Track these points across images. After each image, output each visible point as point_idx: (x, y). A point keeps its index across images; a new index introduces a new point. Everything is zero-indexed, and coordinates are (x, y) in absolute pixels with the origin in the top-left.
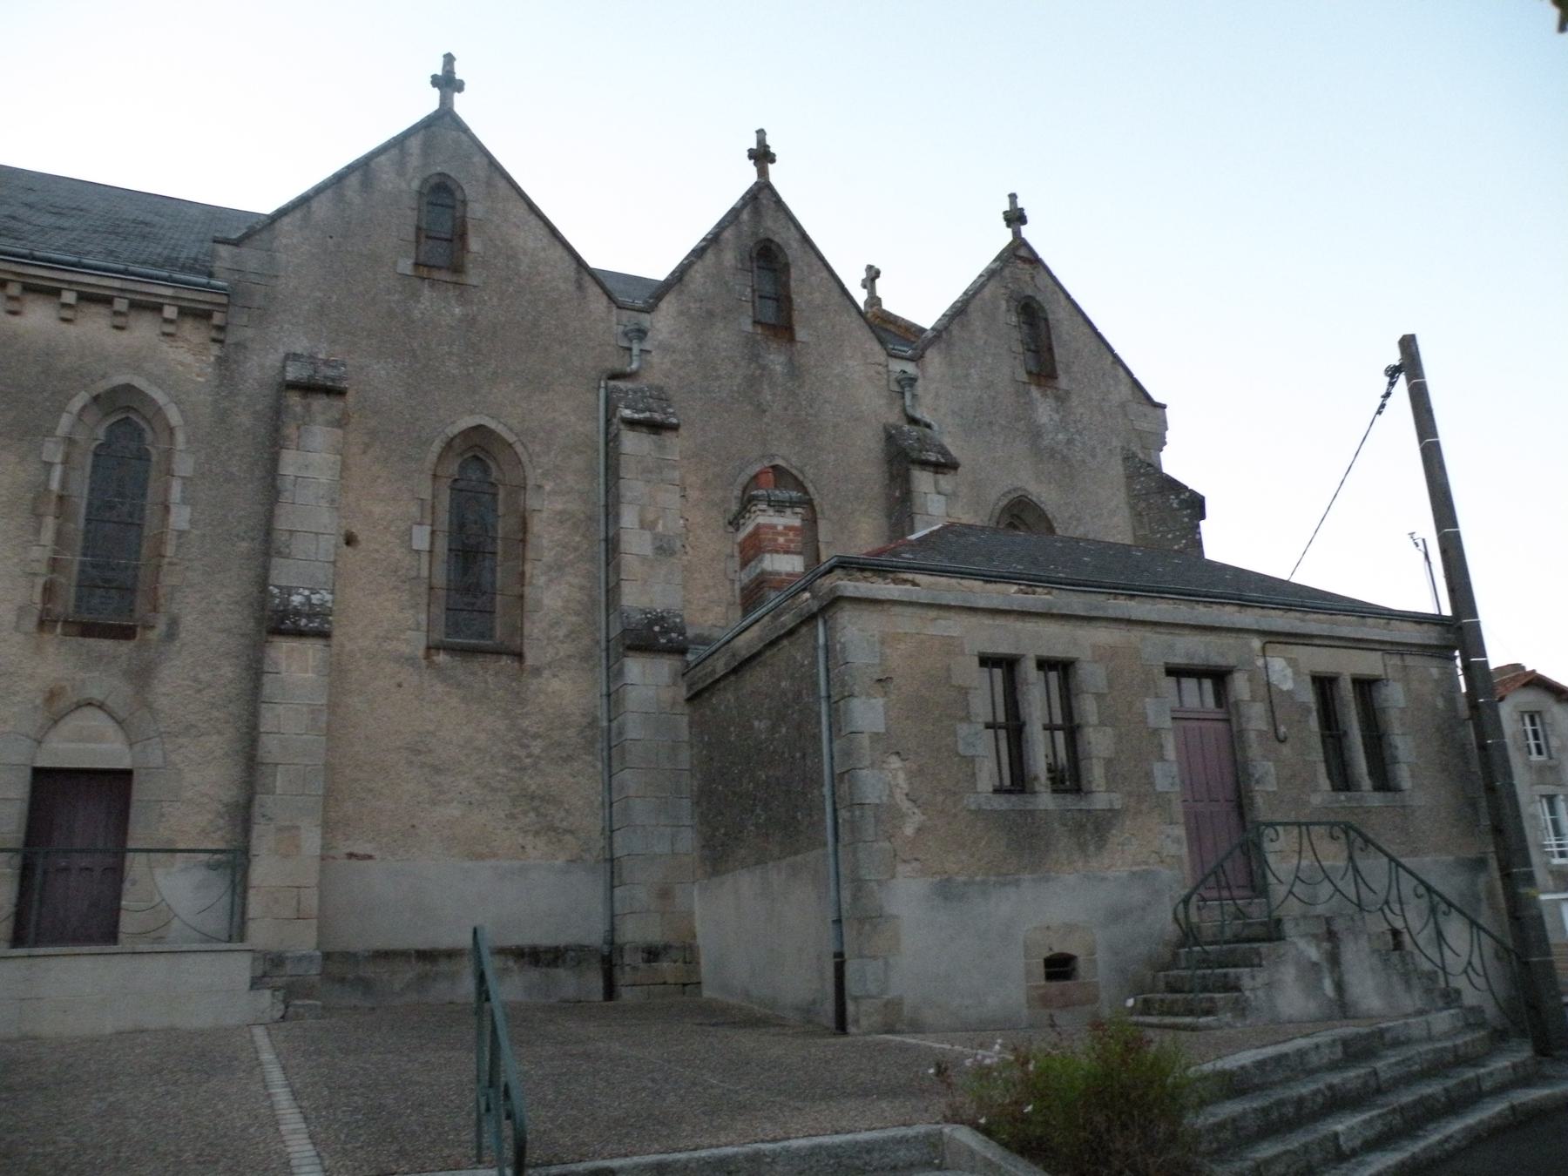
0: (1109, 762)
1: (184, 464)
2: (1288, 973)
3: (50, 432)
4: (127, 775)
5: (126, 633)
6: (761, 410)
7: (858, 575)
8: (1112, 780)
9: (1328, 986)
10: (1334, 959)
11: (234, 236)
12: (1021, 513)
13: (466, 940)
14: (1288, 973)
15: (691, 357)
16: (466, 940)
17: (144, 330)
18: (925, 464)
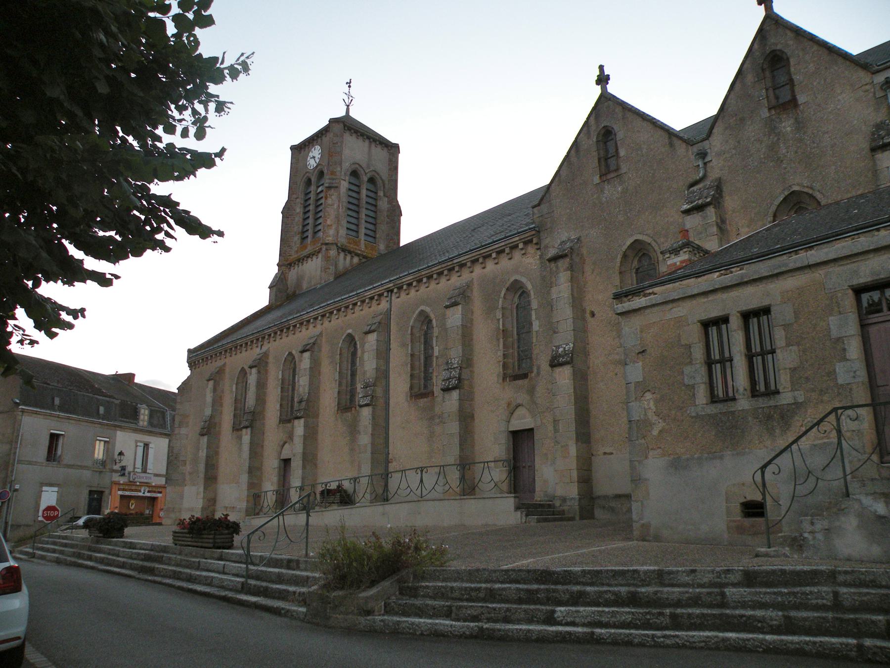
0: (793, 370)
3: (497, 308)
4: (532, 429)
5: (525, 376)
6: (780, 161)
7: (625, 299)
8: (795, 386)
11: (704, 136)
12: (795, 202)
15: (734, 152)
17: (490, 265)
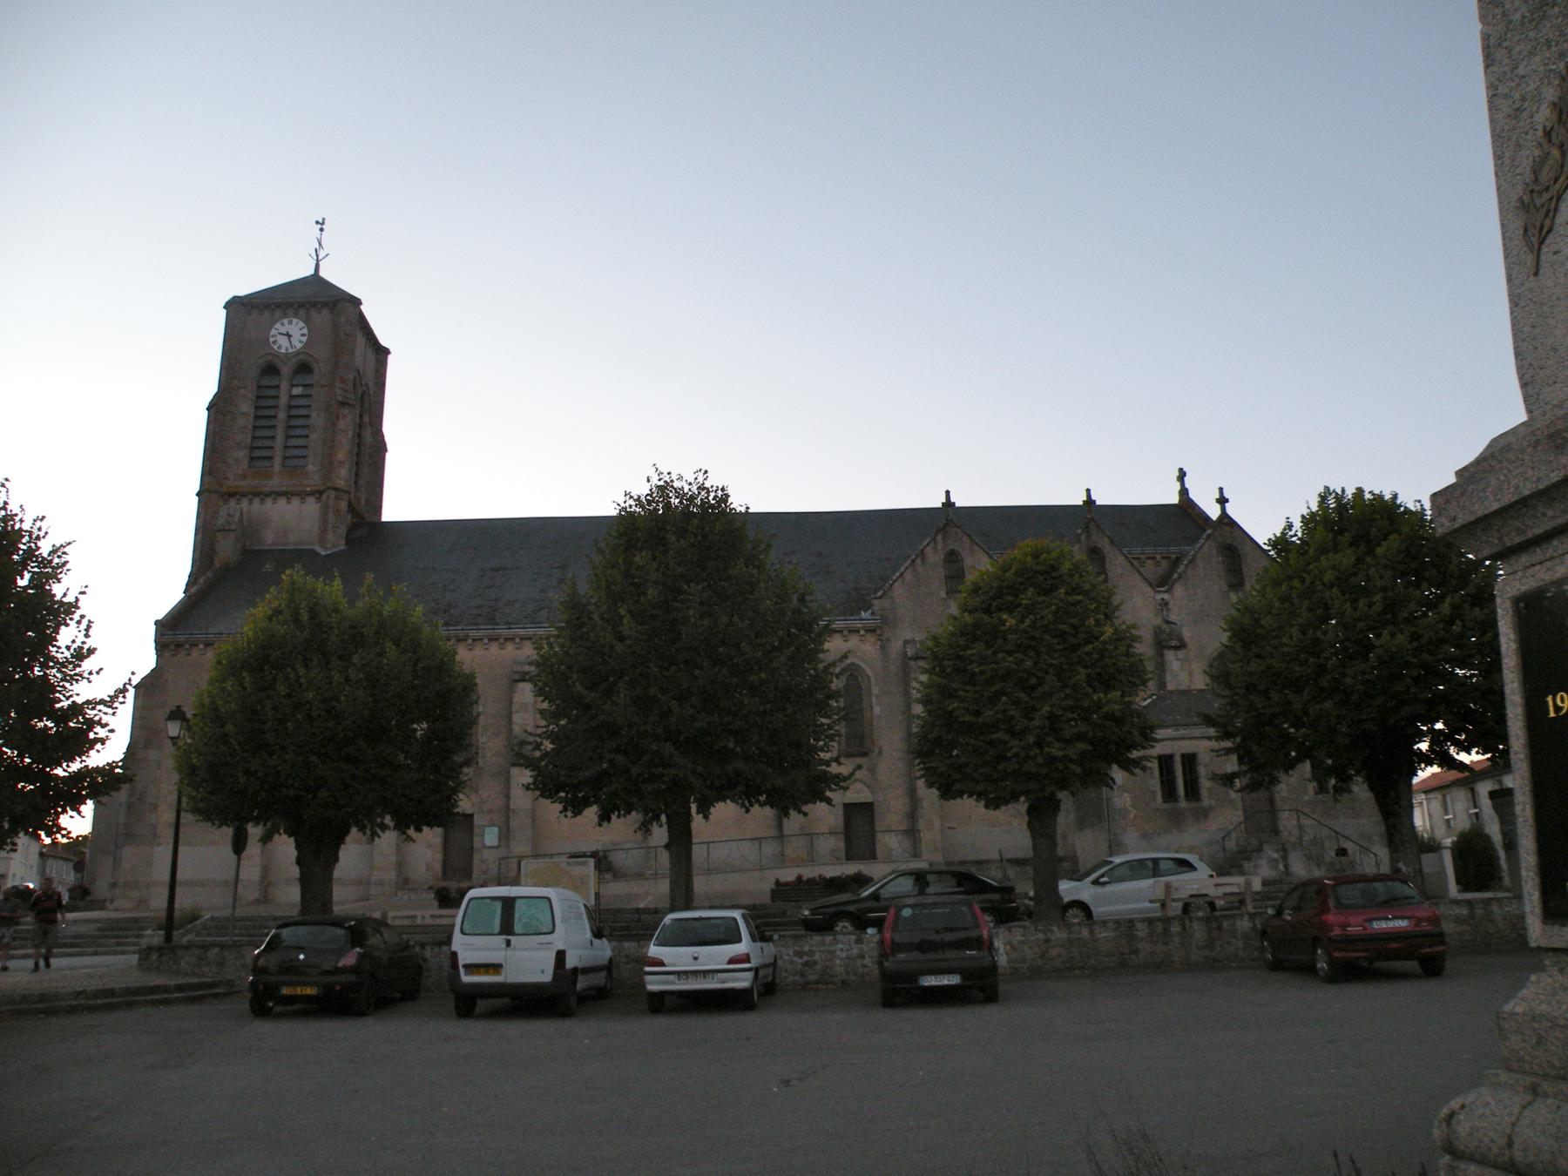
1: (875, 690)
2: (1264, 862)
8: (1210, 798)
9: (1281, 867)
10: (1285, 858)
13: (997, 856)
14: (1264, 862)
16: (997, 856)
18: (1171, 648)
